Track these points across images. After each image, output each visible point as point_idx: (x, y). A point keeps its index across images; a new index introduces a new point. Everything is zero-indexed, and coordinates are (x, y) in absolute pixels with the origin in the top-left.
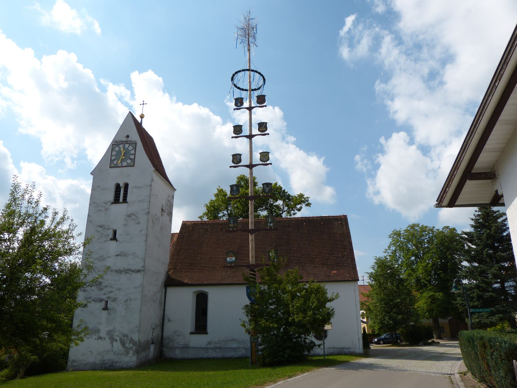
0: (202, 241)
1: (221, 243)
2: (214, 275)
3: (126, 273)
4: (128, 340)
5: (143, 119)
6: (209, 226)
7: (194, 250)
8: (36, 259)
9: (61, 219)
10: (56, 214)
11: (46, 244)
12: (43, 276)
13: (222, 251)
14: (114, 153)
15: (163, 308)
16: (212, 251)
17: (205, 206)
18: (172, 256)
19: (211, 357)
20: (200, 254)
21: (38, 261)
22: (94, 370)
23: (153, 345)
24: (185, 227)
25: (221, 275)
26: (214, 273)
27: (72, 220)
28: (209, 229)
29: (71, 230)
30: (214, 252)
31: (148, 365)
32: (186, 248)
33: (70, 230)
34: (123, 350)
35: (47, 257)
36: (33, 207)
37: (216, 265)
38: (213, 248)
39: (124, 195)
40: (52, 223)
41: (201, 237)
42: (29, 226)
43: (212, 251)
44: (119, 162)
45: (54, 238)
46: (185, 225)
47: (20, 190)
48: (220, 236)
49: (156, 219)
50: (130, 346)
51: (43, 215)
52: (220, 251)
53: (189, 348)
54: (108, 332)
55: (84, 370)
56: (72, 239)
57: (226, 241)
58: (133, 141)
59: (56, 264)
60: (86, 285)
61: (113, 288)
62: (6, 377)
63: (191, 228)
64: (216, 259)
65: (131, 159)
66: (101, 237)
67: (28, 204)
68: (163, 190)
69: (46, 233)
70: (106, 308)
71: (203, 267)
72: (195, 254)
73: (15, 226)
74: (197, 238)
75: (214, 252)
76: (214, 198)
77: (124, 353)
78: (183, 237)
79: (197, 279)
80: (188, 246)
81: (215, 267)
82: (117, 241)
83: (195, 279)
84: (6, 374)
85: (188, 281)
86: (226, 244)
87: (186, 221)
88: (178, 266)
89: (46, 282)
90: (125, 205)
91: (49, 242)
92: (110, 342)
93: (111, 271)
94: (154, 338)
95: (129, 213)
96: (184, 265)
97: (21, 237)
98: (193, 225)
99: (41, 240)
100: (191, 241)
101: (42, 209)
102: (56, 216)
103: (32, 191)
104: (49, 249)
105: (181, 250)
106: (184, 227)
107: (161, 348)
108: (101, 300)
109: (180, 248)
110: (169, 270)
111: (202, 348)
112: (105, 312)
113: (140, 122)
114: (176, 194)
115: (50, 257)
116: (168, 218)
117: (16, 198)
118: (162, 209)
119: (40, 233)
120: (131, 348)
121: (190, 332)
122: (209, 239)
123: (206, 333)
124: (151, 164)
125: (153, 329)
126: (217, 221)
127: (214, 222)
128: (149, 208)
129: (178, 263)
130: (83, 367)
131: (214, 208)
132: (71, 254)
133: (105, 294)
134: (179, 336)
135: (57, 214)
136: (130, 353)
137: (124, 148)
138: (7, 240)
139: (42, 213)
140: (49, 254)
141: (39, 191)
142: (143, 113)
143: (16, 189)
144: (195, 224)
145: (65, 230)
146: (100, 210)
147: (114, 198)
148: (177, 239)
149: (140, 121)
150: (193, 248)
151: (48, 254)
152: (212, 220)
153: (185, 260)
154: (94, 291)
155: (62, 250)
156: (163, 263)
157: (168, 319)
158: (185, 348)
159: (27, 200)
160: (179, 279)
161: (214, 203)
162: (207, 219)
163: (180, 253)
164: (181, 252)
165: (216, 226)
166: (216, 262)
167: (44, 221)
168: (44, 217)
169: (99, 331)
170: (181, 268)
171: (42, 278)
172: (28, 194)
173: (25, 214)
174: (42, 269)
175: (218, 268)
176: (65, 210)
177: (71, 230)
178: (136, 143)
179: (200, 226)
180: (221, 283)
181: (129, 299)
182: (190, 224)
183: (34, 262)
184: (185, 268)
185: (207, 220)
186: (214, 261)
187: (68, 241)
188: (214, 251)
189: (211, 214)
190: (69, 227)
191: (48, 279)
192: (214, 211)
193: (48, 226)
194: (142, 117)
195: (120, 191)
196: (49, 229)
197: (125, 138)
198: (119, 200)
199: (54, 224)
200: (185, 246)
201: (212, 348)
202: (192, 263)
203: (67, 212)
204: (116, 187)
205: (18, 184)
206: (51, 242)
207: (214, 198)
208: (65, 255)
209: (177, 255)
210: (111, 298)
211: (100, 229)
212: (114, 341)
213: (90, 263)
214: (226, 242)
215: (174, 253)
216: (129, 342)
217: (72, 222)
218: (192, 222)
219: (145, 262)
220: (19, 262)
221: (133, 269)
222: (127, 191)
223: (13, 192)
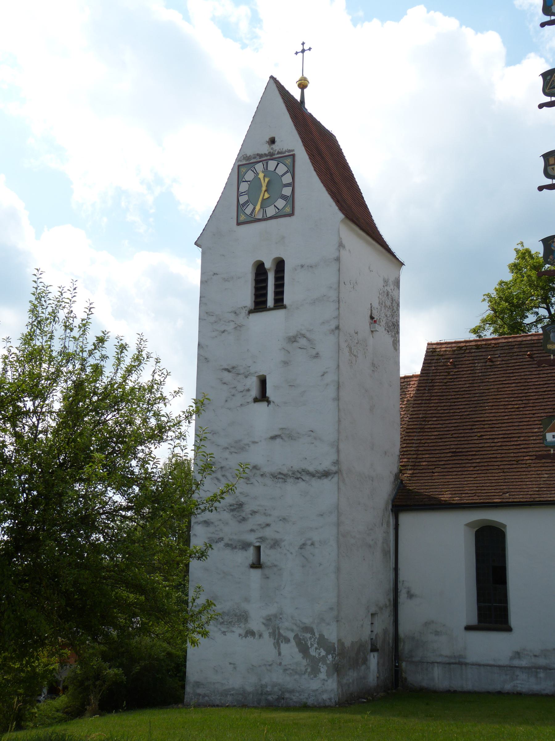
0: (482, 391)
1: (532, 394)
2: (517, 480)
3: (298, 478)
4: (315, 639)
5: (305, 90)
6: (498, 352)
7: (462, 417)
8: (92, 452)
9: (135, 360)
10: (122, 350)
11: (110, 417)
12: (109, 488)
13: (536, 415)
14: (244, 187)
15: (392, 565)
16: (510, 417)
17: (484, 300)
18: (407, 434)
19: (524, 690)
20: (477, 427)
21: (97, 455)
22: (244, 706)
23: (376, 654)
24: (436, 358)
25: (538, 479)
26: (519, 474)
27: (158, 361)
28: (499, 359)
29: (158, 384)
30: (515, 420)
31: (365, 700)
32: (441, 412)
33: (156, 384)
34: (304, 662)
35: (114, 448)
36: (74, 338)
37: (524, 454)
38: (513, 410)
39: (276, 290)
40: (117, 369)
41: (479, 381)
42: (72, 380)
43: (510, 417)
44: (258, 207)
45: (124, 404)
46: (434, 354)
47: (48, 302)
48: (529, 377)
49: (357, 343)
50: (319, 654)
51: (97, 354)
52: (532, 416)
53: (466, 664)
54: (267, 620)
55: (222, 706)
56: (161, 405)
57: (544, 389)
58: (285, 153)
59: (134, 463)
60: (200, 508)
61: (270, 515)
62: (63, 713)
63: (451, 361)
64: (522, 438)
65: (284, 197)
66: (233, 395)
67: (66, 331)
68: (369, 268)
69: (106, 394)
70: (257, 565)
71: (488, 460)
72: (465, 427)
73: (43, 382)
74: (468, 385)
75: (515, 420)
76: (509, 277)
77: (306, 669)
78: (431, 385)
79: (474, 491)
80: (444, 406)
81: (519, 459)
82: (269, 402)
83: (469, 492)
84: (65, 706)
85: (450, 496)
86: (546, 397)
87: (437, 344)
88: (424, 460)
89: (115, 503)
90: (280, 313)
91: (115, 413)
92: (274, 644)
93: (262, 475)
94: (376, 638)
95: (292, 333)
96: (440, 455)
97: (57, 406)
98: (456, 352)
99: (97, 409)
100: (453, 394)
101: (94, 340)
102: (123, 355)
103: (70, 301)
104: (115, 430)
105: (427, 419)
106: (431, 358)
107: (395, 663)
108: (245, 546)
109: (424, 412)
110: (401, 471)
111: (499, 666)
112: (256, 574)
113: (299, 100)
114: (405, 275)
115: (119, 447)
116: (388, 339)
117: (42, 320)
118: (372, 318)
119: (95, 393)
120: (323, 659)
121: (464, 624)
122: (501, 386)
123: (509, 629)
124: (334, 204)
125: (373, 615)
126: (520, 337)
127: (510, 340)
128: (338, 317)
129: (424, 452)
130: (219, 698)
131: (510, 303)
132: (162, 438)
133: (252, 531)
134: (437, 633)
135: (126, 350)
136: (322, 670)
137: (266, 169)
138: (31, 413)
139: (95, 349)
140: (117, 439)
141: (88, 301)
142: (305, 75)
143: (41, 300)
144: (460, 348)
145: (145, 384)
146: (224, 332)
147: (253, 299)
148: (418, 390)
149: (298, 98)
150: (458, 411)
151: (115, 439)
152: (507, 334)
153: (441, 444)
154: (227, 524)
155: (143, 430)
156: (386, 453)
157: (408, 592)
158: (455, 663)
159: (64, 321)
160: (427, 491)
161: (510, 288)
162: (493, 333)
163: (426, 427)
164: (430, 423)
165: (515, 350)
166: (522, 446)
167: (101, 366)
168: (99, 358)
169: (247, 618)
170: (430, 463)
171: (107, 493)
172: (64, 307)
173: (60, 354)
174: (106, 474)
175: (528, 462)
176: (142, 339)
177: (158, 384)
178: (293, 155)
179: (473, 354)
180: (537, 499)
181: (309, 542)
182: (448, 349)
183: (89, 458)
184: (443, 463)
185: (495, 336)
186: (516, 443)
187: (154, 408)
188: (514, 417)
189: (502, 319)
190: (153, 376)
191: (119, 495)
192: (512, 312)
193: (108, 377)
194: (303, 85)
195: (266, 280)
196: (112, 385)
197: (267, 145)
198: (265, 302)
199: (121, 373)
200: (439, 408)
201: (525, 668)
202: (458, 450)
203: (145, 343)
204: (255, 271)
205: (45, 289)
206: (118, 413)
207: (509, 277)
208: (151, 441)
209: (420, 432)
210: (267, 539)
211: (227, 376)
212: (282, 642)
213: (205, 456)
214: (547, 393)
215: (412, 427)
216: (316, 645)
217: (158, 364)
218: (453, 345)
219: (338, 451)
220: (59, 459)
221: (311, 469)
222: (282, 278)
223: (35, 306)
